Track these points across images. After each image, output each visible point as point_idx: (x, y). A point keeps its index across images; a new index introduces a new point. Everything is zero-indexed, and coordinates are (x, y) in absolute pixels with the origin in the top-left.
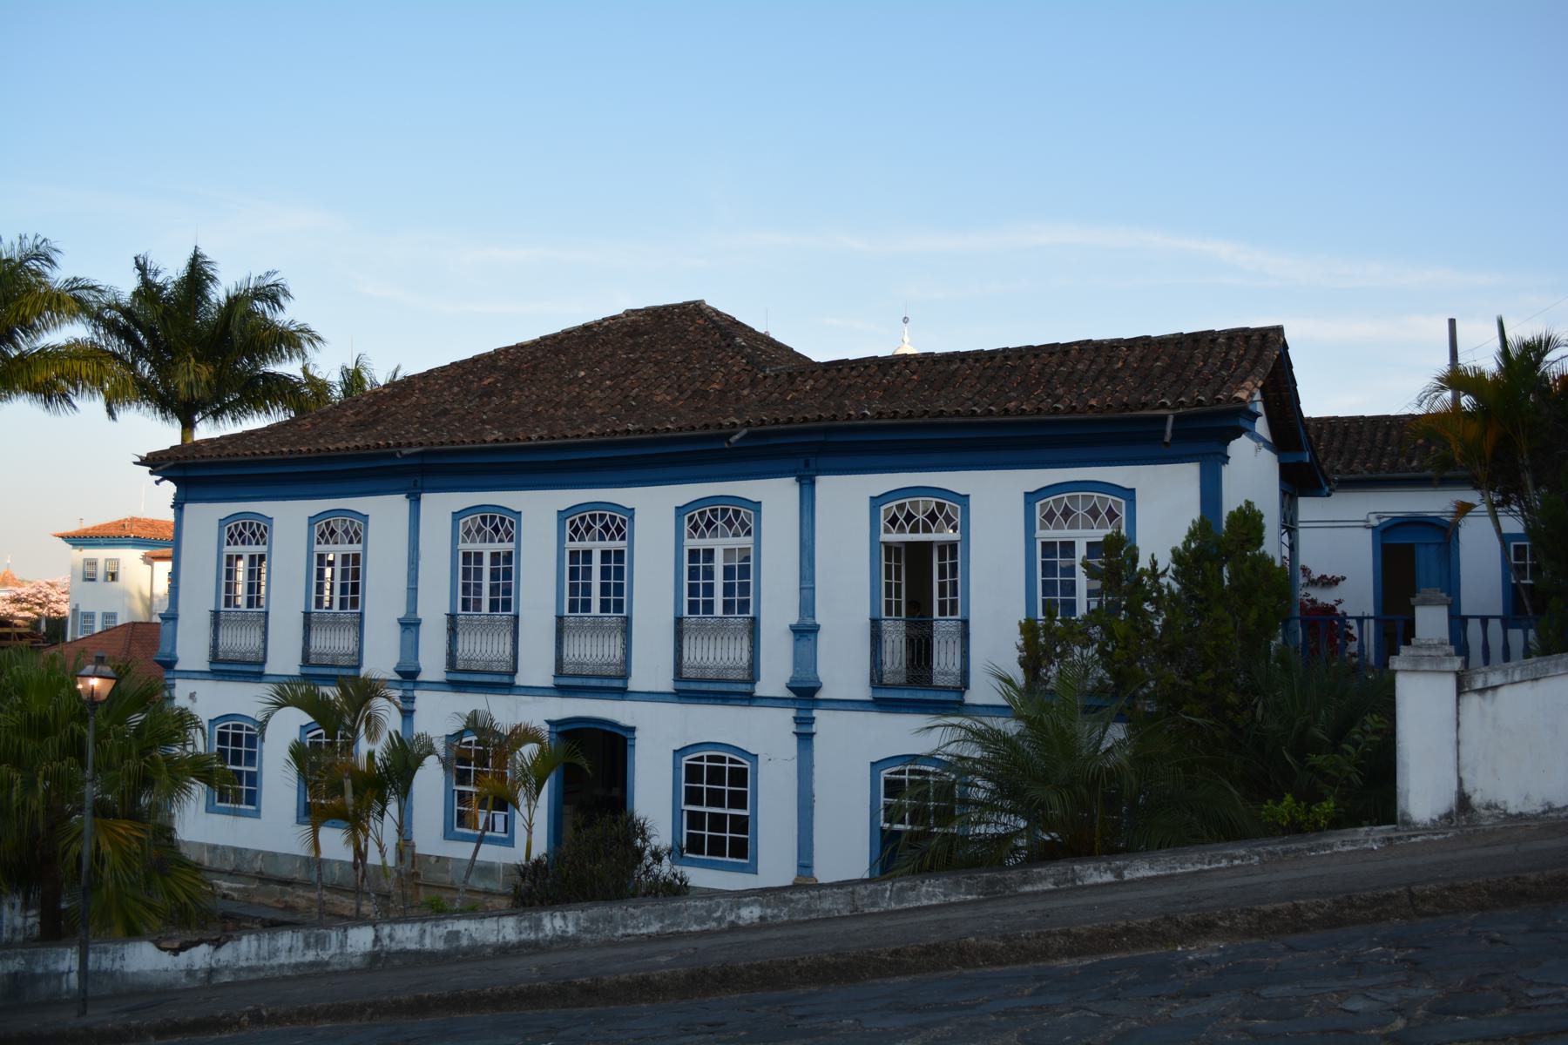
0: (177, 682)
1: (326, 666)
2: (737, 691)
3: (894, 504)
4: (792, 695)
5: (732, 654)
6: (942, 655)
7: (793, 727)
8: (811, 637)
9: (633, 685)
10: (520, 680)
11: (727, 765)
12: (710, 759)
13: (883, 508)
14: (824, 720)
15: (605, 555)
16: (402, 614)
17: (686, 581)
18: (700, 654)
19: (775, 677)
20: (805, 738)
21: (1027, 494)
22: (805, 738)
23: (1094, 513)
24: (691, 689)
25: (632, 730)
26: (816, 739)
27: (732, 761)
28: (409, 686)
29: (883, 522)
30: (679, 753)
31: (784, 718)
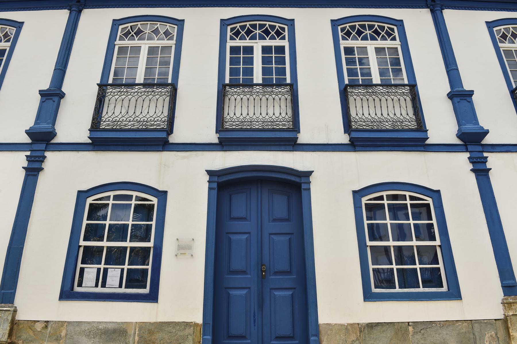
0: (47, 154)
1: (247, 130)
2: (413, 139)
3: (129, 25)
4: (90, 141)
5: (150, 110)
6: (112, 106)
7: (471, 167)
8: (56, 99)
9: (303, 138)
10: (175, 138)
11: (408, 202)
12: (389, 197)
13: (121, 27)
14: (494, 161)
15: (266, 50)
16: (46, 86)
17: (345, 67)
18: (368, 111)
19: (442, 126)
20: (481, 172)
21: (222, 20)
22: (481, 172)
23: (156, 32)
24: (363, 140)
25: (309, 174)
26: (491, 174)
27: (412, 198)
28: (43, 146)
29: (229, 34)
30: (357, 194)
31: (462, 159)
